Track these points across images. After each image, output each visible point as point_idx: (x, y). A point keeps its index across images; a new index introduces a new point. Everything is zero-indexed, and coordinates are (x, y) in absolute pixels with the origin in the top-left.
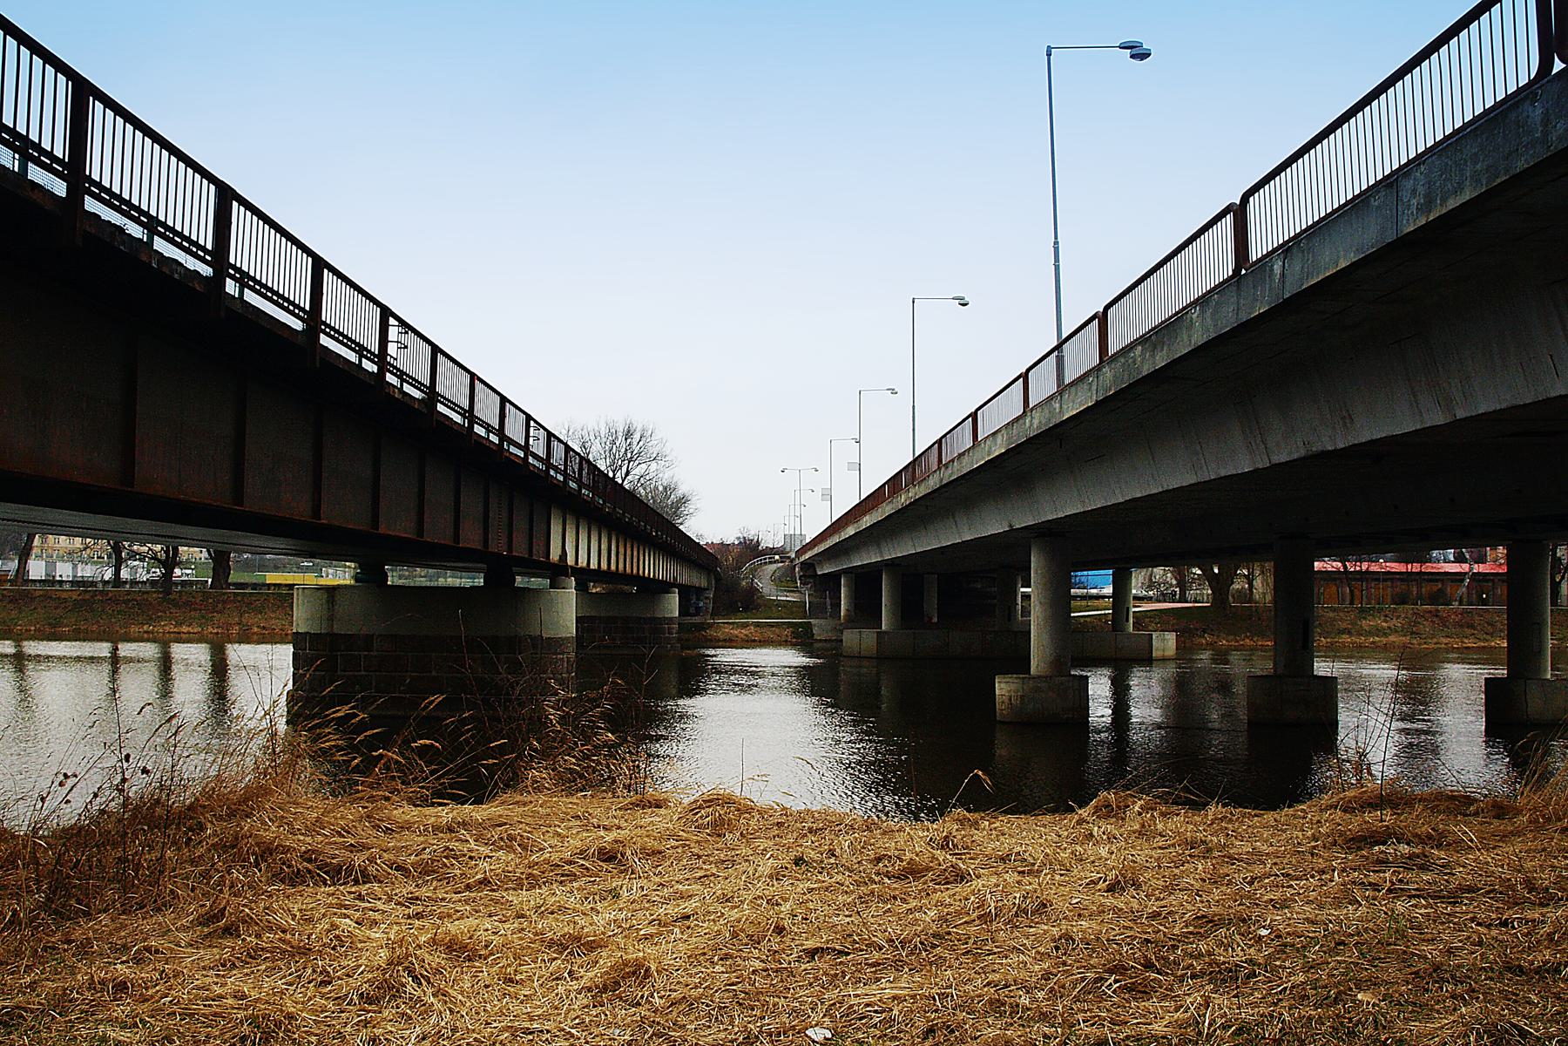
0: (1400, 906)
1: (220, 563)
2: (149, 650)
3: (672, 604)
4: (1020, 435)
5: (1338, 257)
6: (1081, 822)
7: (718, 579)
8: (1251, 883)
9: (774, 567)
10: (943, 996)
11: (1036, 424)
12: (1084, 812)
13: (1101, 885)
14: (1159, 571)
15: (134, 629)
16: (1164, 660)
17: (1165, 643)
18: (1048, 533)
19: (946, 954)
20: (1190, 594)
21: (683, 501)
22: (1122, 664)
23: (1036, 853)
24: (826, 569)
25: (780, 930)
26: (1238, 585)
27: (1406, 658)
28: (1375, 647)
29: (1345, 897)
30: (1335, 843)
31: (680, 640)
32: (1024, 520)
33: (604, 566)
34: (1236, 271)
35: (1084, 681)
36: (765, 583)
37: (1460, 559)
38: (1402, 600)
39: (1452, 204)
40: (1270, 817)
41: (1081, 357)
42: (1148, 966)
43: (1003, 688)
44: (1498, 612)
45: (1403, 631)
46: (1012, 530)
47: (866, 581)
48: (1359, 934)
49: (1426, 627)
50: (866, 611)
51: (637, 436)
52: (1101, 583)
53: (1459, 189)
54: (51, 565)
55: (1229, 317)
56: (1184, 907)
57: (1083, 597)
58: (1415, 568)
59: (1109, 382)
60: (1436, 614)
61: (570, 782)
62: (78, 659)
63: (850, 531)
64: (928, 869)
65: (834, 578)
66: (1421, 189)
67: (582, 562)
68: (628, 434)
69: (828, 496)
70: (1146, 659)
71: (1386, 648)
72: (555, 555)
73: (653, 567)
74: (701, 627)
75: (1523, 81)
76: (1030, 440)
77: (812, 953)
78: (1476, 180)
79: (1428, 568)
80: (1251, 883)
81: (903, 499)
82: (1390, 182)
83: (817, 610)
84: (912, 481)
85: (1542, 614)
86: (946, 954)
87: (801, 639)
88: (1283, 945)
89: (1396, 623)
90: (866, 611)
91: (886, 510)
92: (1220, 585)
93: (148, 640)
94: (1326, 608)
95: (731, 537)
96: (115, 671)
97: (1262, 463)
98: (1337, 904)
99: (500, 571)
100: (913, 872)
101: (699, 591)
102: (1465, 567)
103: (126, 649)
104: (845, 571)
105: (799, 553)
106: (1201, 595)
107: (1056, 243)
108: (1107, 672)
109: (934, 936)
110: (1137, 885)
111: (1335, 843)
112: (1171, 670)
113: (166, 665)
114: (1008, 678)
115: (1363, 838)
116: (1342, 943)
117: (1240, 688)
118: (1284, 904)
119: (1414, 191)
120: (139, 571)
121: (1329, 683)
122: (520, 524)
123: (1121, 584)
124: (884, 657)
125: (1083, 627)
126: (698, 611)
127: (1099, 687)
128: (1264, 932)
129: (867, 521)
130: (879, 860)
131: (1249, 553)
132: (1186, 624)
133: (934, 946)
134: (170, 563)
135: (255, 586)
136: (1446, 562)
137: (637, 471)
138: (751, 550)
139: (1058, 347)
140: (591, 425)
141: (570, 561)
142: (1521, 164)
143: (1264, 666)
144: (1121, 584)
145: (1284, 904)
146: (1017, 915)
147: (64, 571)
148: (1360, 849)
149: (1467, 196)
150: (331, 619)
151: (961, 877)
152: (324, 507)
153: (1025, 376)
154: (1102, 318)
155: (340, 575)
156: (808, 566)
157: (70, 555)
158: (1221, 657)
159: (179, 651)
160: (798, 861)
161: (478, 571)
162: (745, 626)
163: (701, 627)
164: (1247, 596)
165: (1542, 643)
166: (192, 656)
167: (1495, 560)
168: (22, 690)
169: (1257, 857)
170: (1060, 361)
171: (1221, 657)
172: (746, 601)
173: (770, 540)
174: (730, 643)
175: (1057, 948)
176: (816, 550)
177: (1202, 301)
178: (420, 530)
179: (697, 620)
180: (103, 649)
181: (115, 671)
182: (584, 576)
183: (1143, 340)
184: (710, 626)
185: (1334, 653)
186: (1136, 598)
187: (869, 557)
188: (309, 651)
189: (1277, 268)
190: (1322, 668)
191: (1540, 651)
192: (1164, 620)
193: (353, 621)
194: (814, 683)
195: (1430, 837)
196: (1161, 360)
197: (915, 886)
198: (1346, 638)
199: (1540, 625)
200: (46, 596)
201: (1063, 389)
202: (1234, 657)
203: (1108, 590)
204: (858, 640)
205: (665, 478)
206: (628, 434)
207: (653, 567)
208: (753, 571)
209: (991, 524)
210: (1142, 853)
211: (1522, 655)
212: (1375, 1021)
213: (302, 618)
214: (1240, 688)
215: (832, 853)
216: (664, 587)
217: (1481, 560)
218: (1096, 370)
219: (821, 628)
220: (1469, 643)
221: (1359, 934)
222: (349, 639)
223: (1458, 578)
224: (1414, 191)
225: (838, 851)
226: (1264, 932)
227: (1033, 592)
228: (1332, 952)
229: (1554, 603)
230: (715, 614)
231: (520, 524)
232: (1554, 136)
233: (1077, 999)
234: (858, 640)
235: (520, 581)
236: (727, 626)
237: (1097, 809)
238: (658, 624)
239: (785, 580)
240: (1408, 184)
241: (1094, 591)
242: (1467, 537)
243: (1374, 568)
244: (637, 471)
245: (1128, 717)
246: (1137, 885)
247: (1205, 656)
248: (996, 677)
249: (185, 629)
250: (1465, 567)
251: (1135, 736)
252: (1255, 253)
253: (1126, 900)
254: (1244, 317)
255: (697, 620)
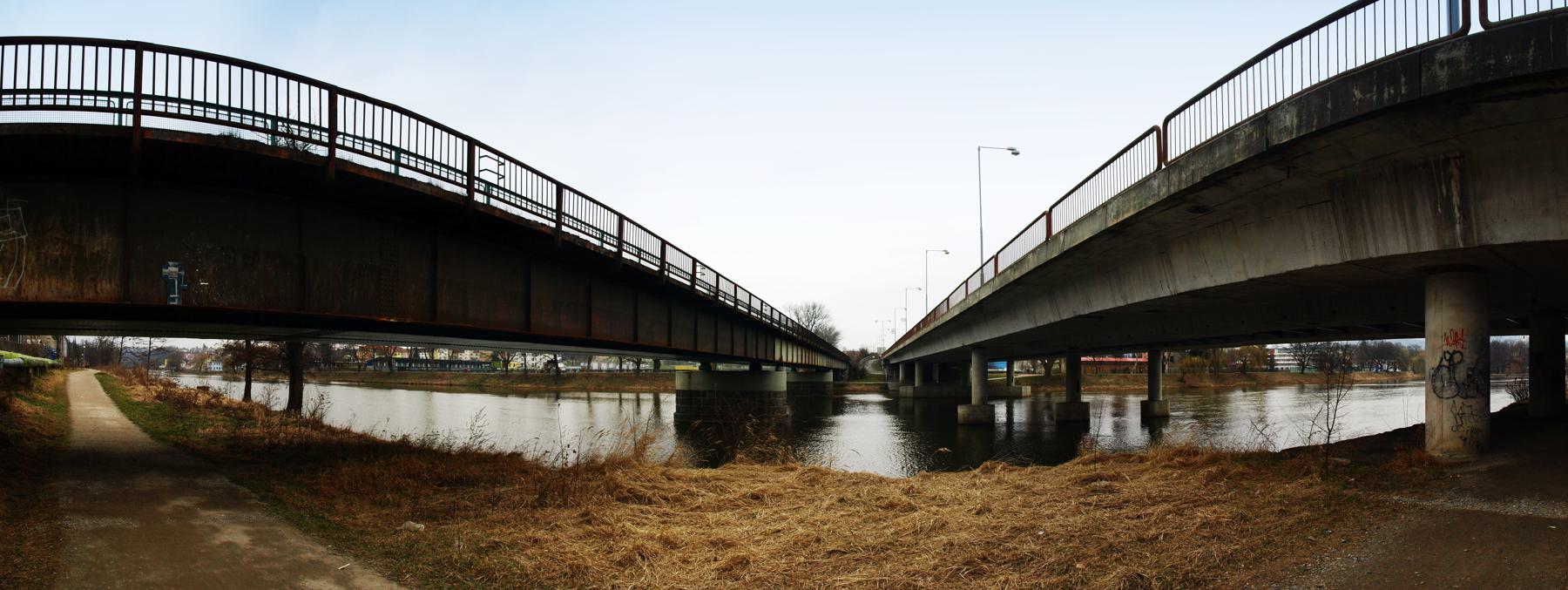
0: (1098, 514)
1: (657, 364)
2: (632, 396)
3: (830, 377)
4: (964, 307)
5: (1085, 234)
6: (975, 476)
7: (850, 365)
8: (1040, 506)
9: (873, 361)
10: (881, 581)
11: (972, 302)
12: (976, 471)
13: (974, 512)
14: (1025, 362)
15: (626, 387)
16: (1026, 397)
17: (1027, 390)
18: (978, 347)
19: (893, 554)
20: (1037, 371)
21: (837, 334)
22: (1011, 398)
23: (947, 496)
24: (893, 361)
25: (818, 540)
26: (1055, 367)
27: (1116, 393)
28: (1104, 389)
29: (1078, 512)
30: (1076, 483)
31: (833, 390)
32: (969, 341)
33: (799, 361)
34: (1047, 238)
35: (993, 406)
36: (869, 367)
37: (1134, 357)
38: (1114, 371)
39: (1126, 216)
40: (1054, 469)
41: (989, 273)
42: (984, 559)
43: (961, 410)
44: (1145, 376)
45: (1114, 384)
46: (964, 346)
47: (909, 366)
48: (1080, 531)
49: (1122, 381)
50: (909, 379)
51: (817, 308)
52: (1002, 367)
53: (1128, 211)
54: (599, 365)
55: (1044, 258)
56: (1009, 522)
57: (992, 372)
58: (1119, 360)
59: (998, 285)
60: (1125, 377)
61: (763, 458)
62: (609, 399)
63: (902, 346)
64: (898, 505)
65: (897, 365)
66: (1115, 209)
67: (790, 360)
68: (814, 307)
69: (894, 331)
70: (1019, 397)
71: (1108, 389)
72: (777, 357)
73: (821, 361)
74: (843, 385)
75: (1152, 171)
76: (969, 309)
77: (831, 553)
78: (1135, 207)
79: (1123, 360)
80: (1040, 506)
81: (921, 333)
82: (1104, 206)
83: (890, 378)
84: (924, 326)
85: (1158, 377)
86: (893, 554)
87: (883, 390)
88: (1049, 539)
89: (1112, 380)
90: (909, 379)
91: (915, 337)
92: (1048, 367)
93: (631, 392)
94: (1086, 374)
95: (857, 348)
96: (621, 404)
97: (1058, 319)
98: (1074, 515)
99: (756, 365)
100: (891, 506)
101: (843, 371)
102: (1135, 360)
103: (625, 396)
104: (919, 359)
105: (883, 355)
106: (1041, 371)
107: (981, 229)
108: (1005, 401)
109: (889, 544)
110: (989, 510)
111: (1076, 483)
112: (1029, 400)
113: (638, 401)
114: (963, 406)
115: (1087, 480)
116: (1073, 536)
117: (1054, 407)
118: (1051, 517)
119: (1112, 210)
120: (629, 366)
121: (1087, 404)
122: (761, 346)
123: (1010, 367)
124: (916, 398)
125: (994, 384)
126: (842, 379)
127: (1001, 411)
128: (1041, 533)
129: (908, 342)
130: (878, 499)
131: (1059, 354)
132: (1035, 383)
133: (888, 549)
134: (638, 363)
135: (670, 371)
136: (1129, 358)
137: (818, 322)
138: (864, 353)
139: (981, 268)
140: (799, 304)
141: (784, 360)
142: (1151, 203)
143: (1064, 399)
144: (1010, 367)
145: (1051, 517)
146: (930, 530)
147: (604, 366)
148: (1087, 484)
149: (1131, 213)
150: (690, 384)
151: (913, 509)
152: (673, 341)
153: (966, 282)
154: (996, 258)
155: (695, 367)
156: (887, 360)
157: (604, 361)
158: (1048, 395)
159: (642, 396)
160: (841, 500)
161: (747, 364)
162: (861, 385)
163: (843, 385)
164: (1058, 371)
165: (1159, 388)
166: (647, 398)
167: (1144, 357)
168: (591, 411)
169: (1044, 492)
170: (982, 275)
171: (1048, 395)
172: (858, 374)
173: (872, 349)
174: (855, 392)
175: (944, 550)
176: (890, 354)
177: (1033, 251)
178: (716, 349)
179: (841, 382)
180: (616, 395)
181: (621, 404)
182: (793, 366)
183: (1011, 267)
184: (847, 385)
185: (1090, 392)
186: (1016, 372)
187: (908, 357)
188: (684, 399)
189: (1062, 238)
190: (1085, 398)
191: (1158, 391)
192: (1026, 381)
193: (699, 385)
194: (889, 408)
195: (1114, 476)
196: (1017, 275)
197: (890, 514)
198: (1094, 386)
199: (1158, 381)
200: (597, 376)
201: (983, 285)
202: (1053, 395)
203: (1005, 370)
204: (906, 391)
205: (830, 325)
206: (814, 307)
207: (821, 361)
208: (864, 362)
209: (955, 343)
210: (998, 491)
211: (1153, 391)
212: (1082, 581)
213: (679, 383)
214: (1054, 407)
215: (858, 495)
216: (827, 369)
217: (1140, 357)
218: (993, 279)
219: (891, 385)
220: (1136, 387)
221: (1080, 531)
222: (697, 392)
223: (1133, 363)
224: (1112, 210)
225: (861, 495)
226: (1041, 533)
227: (973, 372)
228: (1069, 541)
229: (1163, 372)
230: (848, 381)
231: (761, 346)
232: (1161, 193)
233: (947, 581)
234: (906, 391)
235: (764, 367)
236: (854, 385)
237: (983, 469)
238: (824, 384)
239: (877, 366)
240: (1110, 207)
241: (1000, 370)
242: (1135, 348)
243: (1104, 360)
244: (818, 322)
245: (1013, 419)
246: (989, 510)
247: (1042, 395)
248: (959, 407)
249: (644, 387)
250: (1135, 360)
251: (1016, 428)
252: (1054, 232)
253: (985, 519)
254: (1049, 258)
255: (841, 382)
